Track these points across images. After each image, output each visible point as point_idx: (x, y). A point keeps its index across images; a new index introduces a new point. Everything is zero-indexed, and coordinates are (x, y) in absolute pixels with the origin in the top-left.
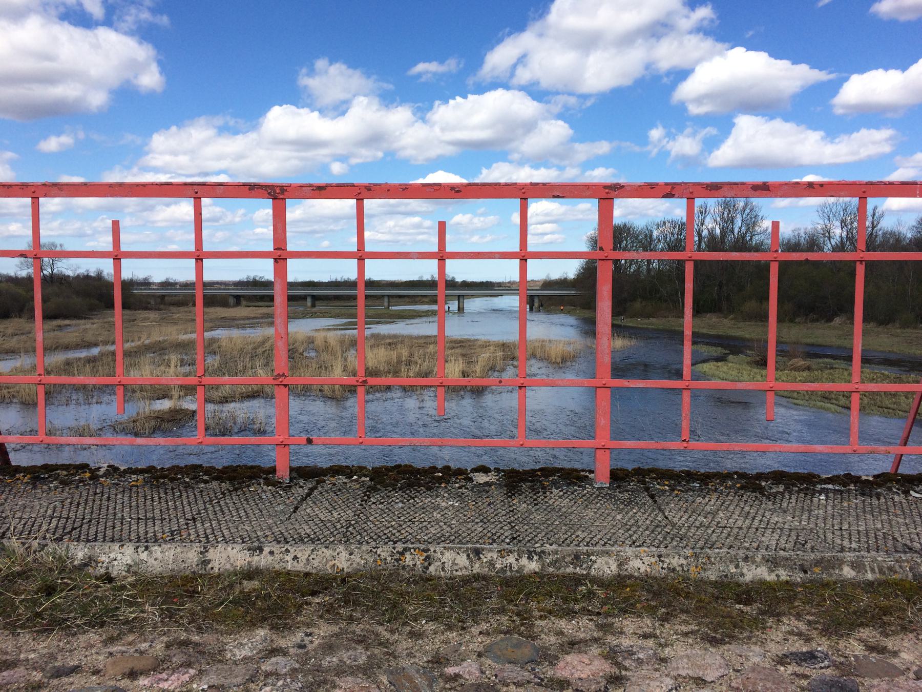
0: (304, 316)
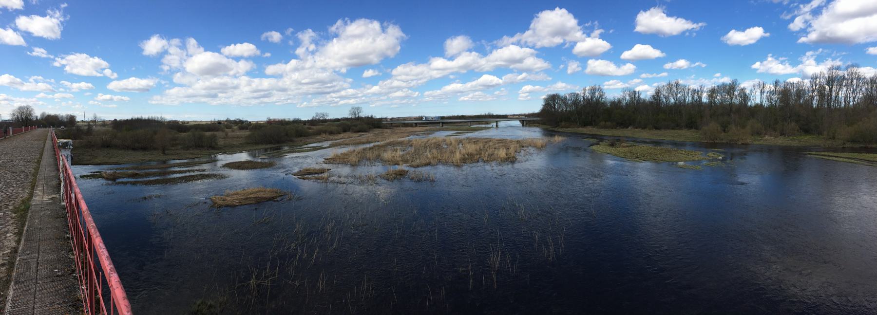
0: (439, 130)
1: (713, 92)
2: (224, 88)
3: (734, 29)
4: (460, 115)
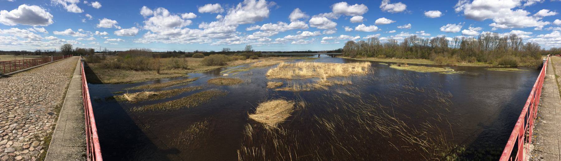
1: (432, 41)
2: (174, 35)
3: (299, 8)
4: (295, 51)
